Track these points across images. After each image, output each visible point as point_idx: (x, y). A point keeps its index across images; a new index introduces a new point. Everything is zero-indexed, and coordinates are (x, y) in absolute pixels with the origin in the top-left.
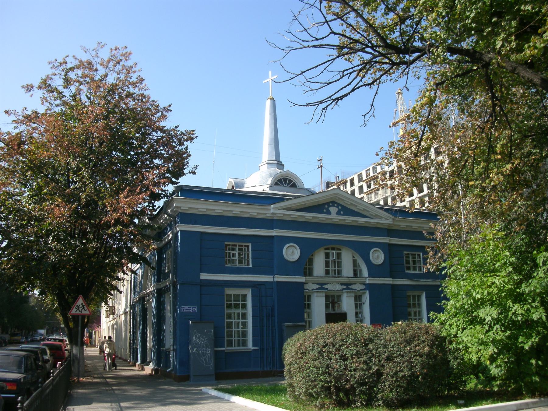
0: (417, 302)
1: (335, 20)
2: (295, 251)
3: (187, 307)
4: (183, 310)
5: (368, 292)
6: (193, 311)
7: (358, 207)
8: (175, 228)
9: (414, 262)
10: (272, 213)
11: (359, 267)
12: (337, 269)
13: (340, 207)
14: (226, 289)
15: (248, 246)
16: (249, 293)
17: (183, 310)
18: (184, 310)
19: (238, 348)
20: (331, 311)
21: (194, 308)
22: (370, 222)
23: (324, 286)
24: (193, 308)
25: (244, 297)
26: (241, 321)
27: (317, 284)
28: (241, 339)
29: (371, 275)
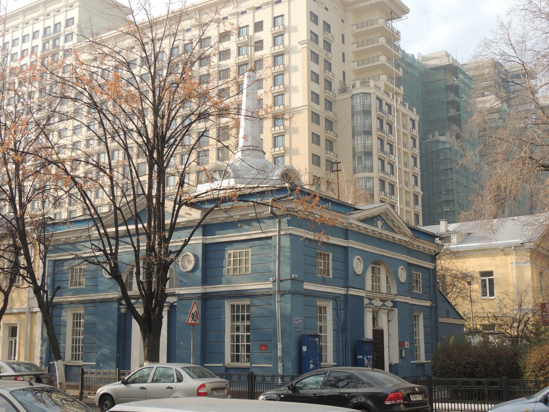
2: (360, 265)
15: (328, 255)
16: (330, 306)
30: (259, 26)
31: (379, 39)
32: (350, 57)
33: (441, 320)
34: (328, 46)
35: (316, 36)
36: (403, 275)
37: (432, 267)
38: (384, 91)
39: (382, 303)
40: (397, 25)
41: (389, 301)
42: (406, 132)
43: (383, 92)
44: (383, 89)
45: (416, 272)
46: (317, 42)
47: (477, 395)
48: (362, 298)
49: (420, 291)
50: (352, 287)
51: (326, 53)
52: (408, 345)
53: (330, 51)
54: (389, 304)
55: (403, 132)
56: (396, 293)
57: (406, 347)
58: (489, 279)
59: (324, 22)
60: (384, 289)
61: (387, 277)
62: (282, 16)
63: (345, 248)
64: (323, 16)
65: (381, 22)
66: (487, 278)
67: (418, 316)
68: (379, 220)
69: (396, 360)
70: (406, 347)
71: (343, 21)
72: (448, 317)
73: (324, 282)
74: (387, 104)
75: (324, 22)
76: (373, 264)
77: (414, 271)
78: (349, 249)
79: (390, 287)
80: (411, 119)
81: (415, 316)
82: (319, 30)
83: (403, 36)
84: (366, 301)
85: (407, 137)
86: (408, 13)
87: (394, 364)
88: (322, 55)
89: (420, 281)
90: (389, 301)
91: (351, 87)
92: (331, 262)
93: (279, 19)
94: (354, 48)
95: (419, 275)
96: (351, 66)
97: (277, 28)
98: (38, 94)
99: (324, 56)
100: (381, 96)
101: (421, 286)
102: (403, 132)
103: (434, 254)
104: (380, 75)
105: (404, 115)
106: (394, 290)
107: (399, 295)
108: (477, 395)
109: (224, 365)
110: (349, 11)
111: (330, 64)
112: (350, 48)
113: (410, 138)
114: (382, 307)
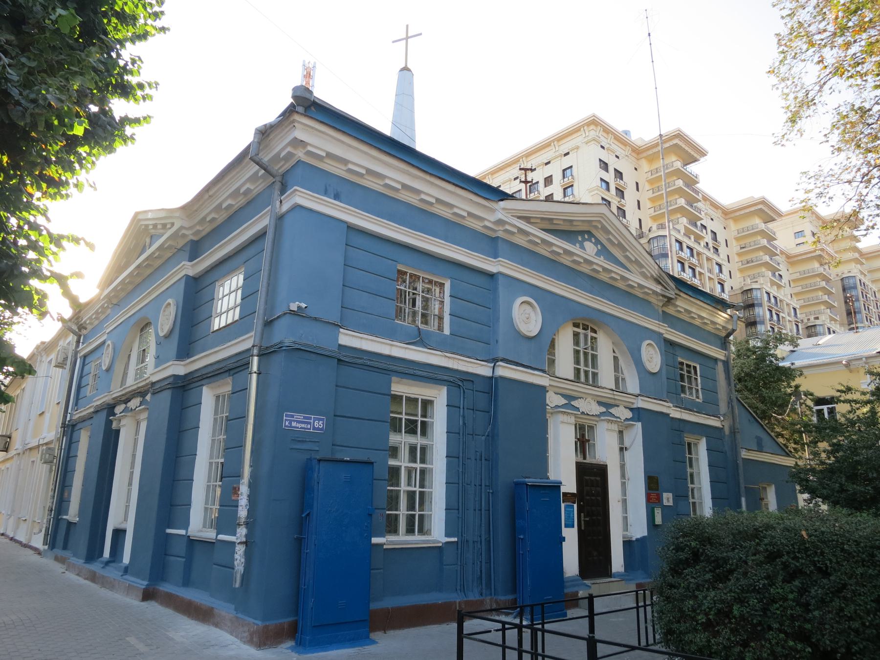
0: (420, 419)
1: (237, 285)
2: (532, 314)
3: (299, 417)
4: (290, 423)
5: (639, 425)
6: (314, 428)
7: (628, 253)
8: (278, 203)
9: (690, 378)
10: (500, 222)
11: (622, 373)
12: (590, 369)
13: (599, 247)
14: (394, 379)
15: (442, 285)
16: (440, 397)
17: (290, 423)
18: (294, 424)
19: (410, 538)
20: (581, 460)
21: (319, 420)
22: (74, 397)
23: (573, 403)
24: (315, 419)
25: (427, 404)
26: (418, 466)
27: (563, 396)
28: (417, 513)
29: (644, 393)
30: (548, 181)
31: (676, 181)
32: (646, 204)
33: (744, 454)
34: (620, 193)
35: (607, 183)
36: (653, 359)
37: (723, 358)
38: (684, 234)
39: (603, 410)
40: (693, 168)
41: (621, 408)
42: (711, 276)
43: (682, 234)
44: (682, 231)
45: (688, 360)
46: (608, 189)
47: (784, 448)
48: (543, 389)
49: (698, 397)
50: (503, 360)
51: (619, 200)
52: (671, 500)
53: (623, 198)
54: (623, 413)
55: (709, 277)
56: (638, 392)
57: (665, 503)
58: (828, 408)
59: (615, 170)
60: (606, 377)
61: (616, 358)
62: (571, 167)
63: (492, 276)
64: (613, 164)
65: (678, 164)
66: (825, 408)
67: (696, 445)
68: (589, 240)
69: (639, 530)
70: (665, 503)
71: (636, 169)
72: (760, 450)
73: (420, 340)
74: (688, 247)
75: (615, 170)
76: (576, 325)
77: (683, 358)
78: (500, 278)
79: (623, 379)
80: (717, 264)
81: (689, 444)
82: (610, 177)
83: (701, 179)
84: (553, 400)
85: (714, 282)
86: (706, 155)
87: (637, 540)
88: (615, 202)
89: (696, 379)
90: (621, 408)
91: (647, 232)
92: (447, 300)
93: (568, 171)
94: (650, 194)
95: (695, 368)
96: (646, 213)
97: (566, 179)
98: (42, 103)
99: (616, 203)
100: (680, 238)
101: (699, 387)
102: (709, 277)
103: (723, 334)
104: (678, 218)
105: (708, 259)
106: (633, 385)
107: (643, 396)
108: (784, 448)
109: (187, 533)
110: (641, 158)
111: (624, 211)
112: (645, 195)
113: (717, 283)
114: (602, 418)
